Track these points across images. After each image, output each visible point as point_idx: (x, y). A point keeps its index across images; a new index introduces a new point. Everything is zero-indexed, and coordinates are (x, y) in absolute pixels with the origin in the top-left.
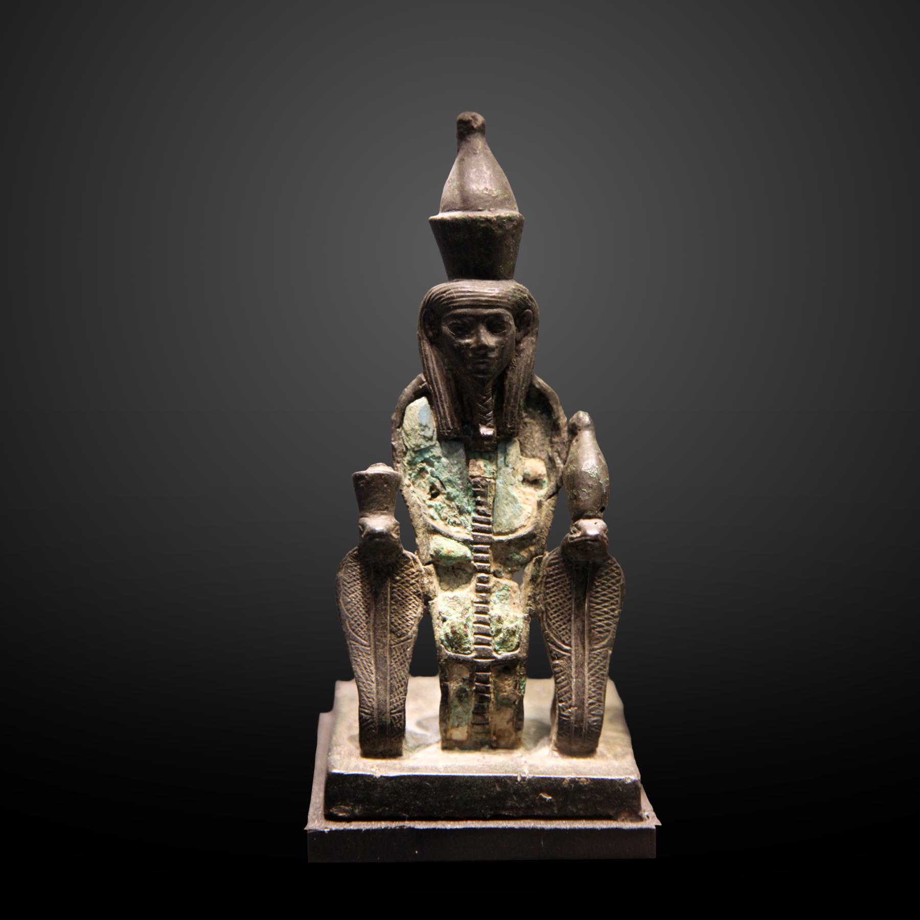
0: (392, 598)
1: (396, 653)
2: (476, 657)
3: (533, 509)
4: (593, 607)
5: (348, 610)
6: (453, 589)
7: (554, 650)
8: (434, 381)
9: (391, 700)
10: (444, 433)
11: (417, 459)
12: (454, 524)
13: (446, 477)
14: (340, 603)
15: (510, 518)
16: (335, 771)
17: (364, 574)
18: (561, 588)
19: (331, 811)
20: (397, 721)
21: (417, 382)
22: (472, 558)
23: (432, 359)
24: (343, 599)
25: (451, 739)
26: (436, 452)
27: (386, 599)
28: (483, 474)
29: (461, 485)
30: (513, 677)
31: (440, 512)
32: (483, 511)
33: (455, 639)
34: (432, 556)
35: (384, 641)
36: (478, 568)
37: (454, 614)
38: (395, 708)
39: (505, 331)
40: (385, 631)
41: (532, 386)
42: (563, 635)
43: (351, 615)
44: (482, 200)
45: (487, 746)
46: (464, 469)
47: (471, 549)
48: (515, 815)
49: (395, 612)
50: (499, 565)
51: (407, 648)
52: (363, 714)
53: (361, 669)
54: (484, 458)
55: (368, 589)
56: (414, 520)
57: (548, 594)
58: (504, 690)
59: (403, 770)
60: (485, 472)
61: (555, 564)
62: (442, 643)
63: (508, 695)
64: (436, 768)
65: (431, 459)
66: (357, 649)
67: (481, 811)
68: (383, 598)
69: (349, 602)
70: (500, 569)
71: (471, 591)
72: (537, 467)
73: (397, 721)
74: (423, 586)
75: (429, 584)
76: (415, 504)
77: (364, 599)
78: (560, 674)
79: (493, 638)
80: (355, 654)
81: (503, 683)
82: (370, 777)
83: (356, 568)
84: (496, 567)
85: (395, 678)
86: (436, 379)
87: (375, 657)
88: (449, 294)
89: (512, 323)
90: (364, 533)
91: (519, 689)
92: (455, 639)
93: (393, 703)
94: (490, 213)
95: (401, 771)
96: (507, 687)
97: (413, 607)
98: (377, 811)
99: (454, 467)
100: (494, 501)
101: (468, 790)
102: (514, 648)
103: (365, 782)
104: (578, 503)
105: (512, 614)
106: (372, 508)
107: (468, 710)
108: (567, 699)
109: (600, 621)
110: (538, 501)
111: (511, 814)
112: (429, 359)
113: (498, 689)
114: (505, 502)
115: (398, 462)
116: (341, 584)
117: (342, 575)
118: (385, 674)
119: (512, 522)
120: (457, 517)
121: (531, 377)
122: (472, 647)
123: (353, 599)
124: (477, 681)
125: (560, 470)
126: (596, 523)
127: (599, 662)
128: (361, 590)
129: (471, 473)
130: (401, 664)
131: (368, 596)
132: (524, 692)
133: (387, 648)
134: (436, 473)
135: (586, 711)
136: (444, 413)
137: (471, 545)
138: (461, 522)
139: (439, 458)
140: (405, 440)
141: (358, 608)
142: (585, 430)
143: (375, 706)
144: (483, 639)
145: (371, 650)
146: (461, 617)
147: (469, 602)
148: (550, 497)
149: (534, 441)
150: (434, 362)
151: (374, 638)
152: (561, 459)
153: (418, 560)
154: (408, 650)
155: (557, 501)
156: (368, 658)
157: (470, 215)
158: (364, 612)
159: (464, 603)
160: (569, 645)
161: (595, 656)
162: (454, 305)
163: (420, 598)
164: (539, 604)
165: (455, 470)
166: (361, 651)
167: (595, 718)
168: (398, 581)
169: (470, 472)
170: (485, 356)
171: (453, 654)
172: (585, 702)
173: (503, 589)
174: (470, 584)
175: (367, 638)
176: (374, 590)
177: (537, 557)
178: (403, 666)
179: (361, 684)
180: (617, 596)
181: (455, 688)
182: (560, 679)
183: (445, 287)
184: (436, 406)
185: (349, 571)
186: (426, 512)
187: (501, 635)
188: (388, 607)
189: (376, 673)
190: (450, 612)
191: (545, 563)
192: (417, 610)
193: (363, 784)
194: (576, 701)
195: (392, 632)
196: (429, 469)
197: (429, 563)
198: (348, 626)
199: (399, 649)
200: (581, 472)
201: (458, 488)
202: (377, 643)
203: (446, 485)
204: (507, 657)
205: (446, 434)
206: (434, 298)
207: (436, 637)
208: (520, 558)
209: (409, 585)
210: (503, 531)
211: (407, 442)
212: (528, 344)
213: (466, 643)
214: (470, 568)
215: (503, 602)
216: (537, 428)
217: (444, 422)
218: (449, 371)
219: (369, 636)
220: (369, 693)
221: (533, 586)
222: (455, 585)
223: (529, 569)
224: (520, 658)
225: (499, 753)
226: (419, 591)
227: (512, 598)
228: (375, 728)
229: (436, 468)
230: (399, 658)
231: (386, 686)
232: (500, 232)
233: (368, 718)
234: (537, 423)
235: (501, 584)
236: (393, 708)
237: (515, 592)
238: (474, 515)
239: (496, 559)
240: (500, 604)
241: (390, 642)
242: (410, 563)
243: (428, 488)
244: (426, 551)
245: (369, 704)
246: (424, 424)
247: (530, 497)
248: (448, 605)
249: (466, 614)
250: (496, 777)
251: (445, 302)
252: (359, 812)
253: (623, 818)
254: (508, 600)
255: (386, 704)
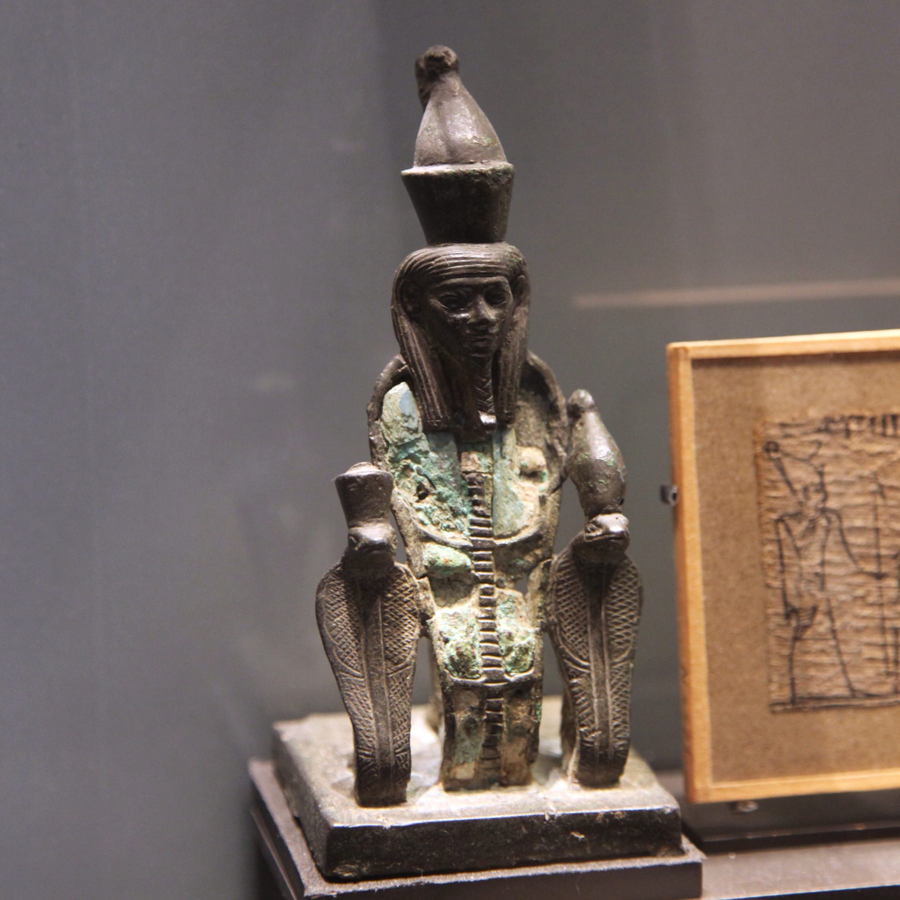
0: (384, 620)
1: (395, 682)
2: (486, 682)
3: (535, 506)
4: (609, 615)
5: (334, 637)
6: (451, 604)
7: (572, 668)
8: (417, 363)
9: (394, 738)
10: (433, 423)
11: (400, 455)
12: (448, 528)
13: (436, 474)
14: (324, 628)
15: (512, 518)
16: (336, 825)
17: (350, 594)
18: (574, 595)
19: (335, 871)
20: (403, 761)
21: (394, 365)
22: (472, 567)
23: (413, 338)
24: (327, 625)
25: (454, 779)
26: (423, 446)
27: (377, 621)
28: (478, 469)
29: (454, 483)
30: (527, 701)
31: (431, 516)
32: (482, 511)
33: (461, 662)
34: (426, 567)
35: (380, 670)
36: (480, 578)
37: (457, 633)
38: (400, 747)
39: (505, 302)
40: (379, 658)
41: (526, 363)
42: (580, 649)
43: (338, 642)
44: (473, 151)
45: (497, 784)
46: (456, 464)
47: (470, 557)
48: (544, 860)
49: (388, 636)
50: (501, 573)
51: (407, 676)
52: (362, 757)
53: (356, 705)
54: (477, 451)
55: (355, 610)
56: (402, 527)
57: (560, 603)
58: (517, 718)
59: (415, 818)
60: (480, 466)
61: (565, 568)
62: (446, 668)
63: (522, 723)
64: (451, 813)
65: (417, 454)
66: (349, 681)
67: (505, 858)
68: (373, 620)
69: (335, 627)
70: (503, 578)
71: (473, 605)
72: (534, 456)
73: (403, 761)
74: (419, 603)
75: (426, 600)
76: (402, 508)
77: (353, 622)
78: (580, 694)
79: (504, 659)
80: (347, 687)
81: (516, 709)
82: (379, 828)
83: (340, 587)
84: (498, 575)
85: (396, 712)
86: (419, 360)
87: (371, 689)
88: (440, 261)
89: (510, 292)
90: (360, 545)
91: (535, 714)
92: (461, 662)
93: (397, 741)
94: (483, 165)
95: (413, 819)
96: (520, 713)
97: (410, 628)
98: (388, 868)
99: (445, 462)
100: (492, 500)
101: (491, 835)
102: (527, 668)
103: (373, 834)
104: (595, 496)
105: (521, 629)
106: (366, 515)
107: (477, 743)
108: (590, 723)
109: (619, 630)
110: (540, 497)
111: (539, 859)
112: (410, 337)
113: (511, 716)
114: (505, 500)
115: (380, 460)
116: (323, 606)
117: (324, 596)
118: (384, 708)
119: (514, 522)
120: (450, 520)
121: (524, 353)
122: (481, 670)
123: (339, 624)
124: (488, 709)
125: (564, 459)
126: (617, 518)
127: (621, 677)
128: (347, 613)
129: (465, 468)
130: (402, 695)
131: (356, 619)
132: (540, 718)
133: (383, 677)
134: (424, 471)
135: (611, 735)
136: (432, 399)
137: (470, 553)
138: (456, 526)
139: (426, 453)
140: (385, 434)
141: (346, 633)
142: (589, 412)
143: (376, 746)
144: (493, 660)
145: (365, 681)
146: (466, 636)
147: (473, 618)
148: (554, 491)
149: (529, 427)
150: (416, 341)
151: (368, 666)
152: (562, 446)
153: (411, 574)
154: (408, 678)
155: (561, 495)
156: (363, 691)
157: (461, 169)
158: (352, 638)
159: (467, 620)
160: (588, 660)
161: (617, 671)
162: (447, 274)
163: (416, 618)
164: (550, 615)
165: (446, 465)
166: (354, 684)
167: (621, 742)
168: (389, 599)
169: (463, 467)
170: (486, 332)
171: (459, 680)
172: (610, 724)
173: (508, 600)
174: (470, 597)
175: (359, 668)
176: (362, 611)
177: (545, 562)
178: (404, 697)
179: (357, 722)
180: (635, 601)
181: (462, 719)
182: (579, 701)
183: (432, 254)
184: (421, 393)
185: (332, 591)
186: (415, 517)
187: (513, 654)
188: (381, 630)
189: (374, 707)
190: (452, 631)
191: (554, 569)
192: (413, 631)
193: (371, 837)
194: (600, 724)
195: (387, 658)
196: (415, 466)
197: (423, 577)
198: (336, 655)
199: (398, 678)
200: (596, 460)
201: (451, 487)
202: (372, 673)
203: (436, 484)
204: (521, 679)
205: (435, 425)
206: (417, 266)
207: (438, 661)
208: (525, 564)
209: (402, 603)
210: (505, 534)
211: (388, 435)
212: (521, 316)
213: (474, 665)
214: (470, 578)
215: (509, 615)
216: (531, 412)
217: (432, 410)
218: (434, 351)
219: (362, 665)
220: (368, 731)
221: (542, 595)
222: (453, 600)
223: (535, 576)
224: (535, 679)
225: (513, 791)
226: (415, 609)
227: (518, 610)
228: (377, 772)
229: (423, 464)
230: (399, 688)
231: (387, 722)
232: (496, 187)
233: (369, 761)
234: (531, 406)
235: (506, 595)
236: (397, 746)
237: (520, 603)
238: (471, 517)
239: (498, 566)
240: (506, 618)
241: (386, 670)
242: (403, 577)
243: (414, 489)
244: (419, 563)
245: (369, 744)
246: (407, 414)
247: (530, 493)
248: (449, 623)
249: (471, 632)
250: (521, 817)
251: (435, 271)
252: (367, 870)
253: (663, 853)
254: (515, 614)
255: (389, 743)
